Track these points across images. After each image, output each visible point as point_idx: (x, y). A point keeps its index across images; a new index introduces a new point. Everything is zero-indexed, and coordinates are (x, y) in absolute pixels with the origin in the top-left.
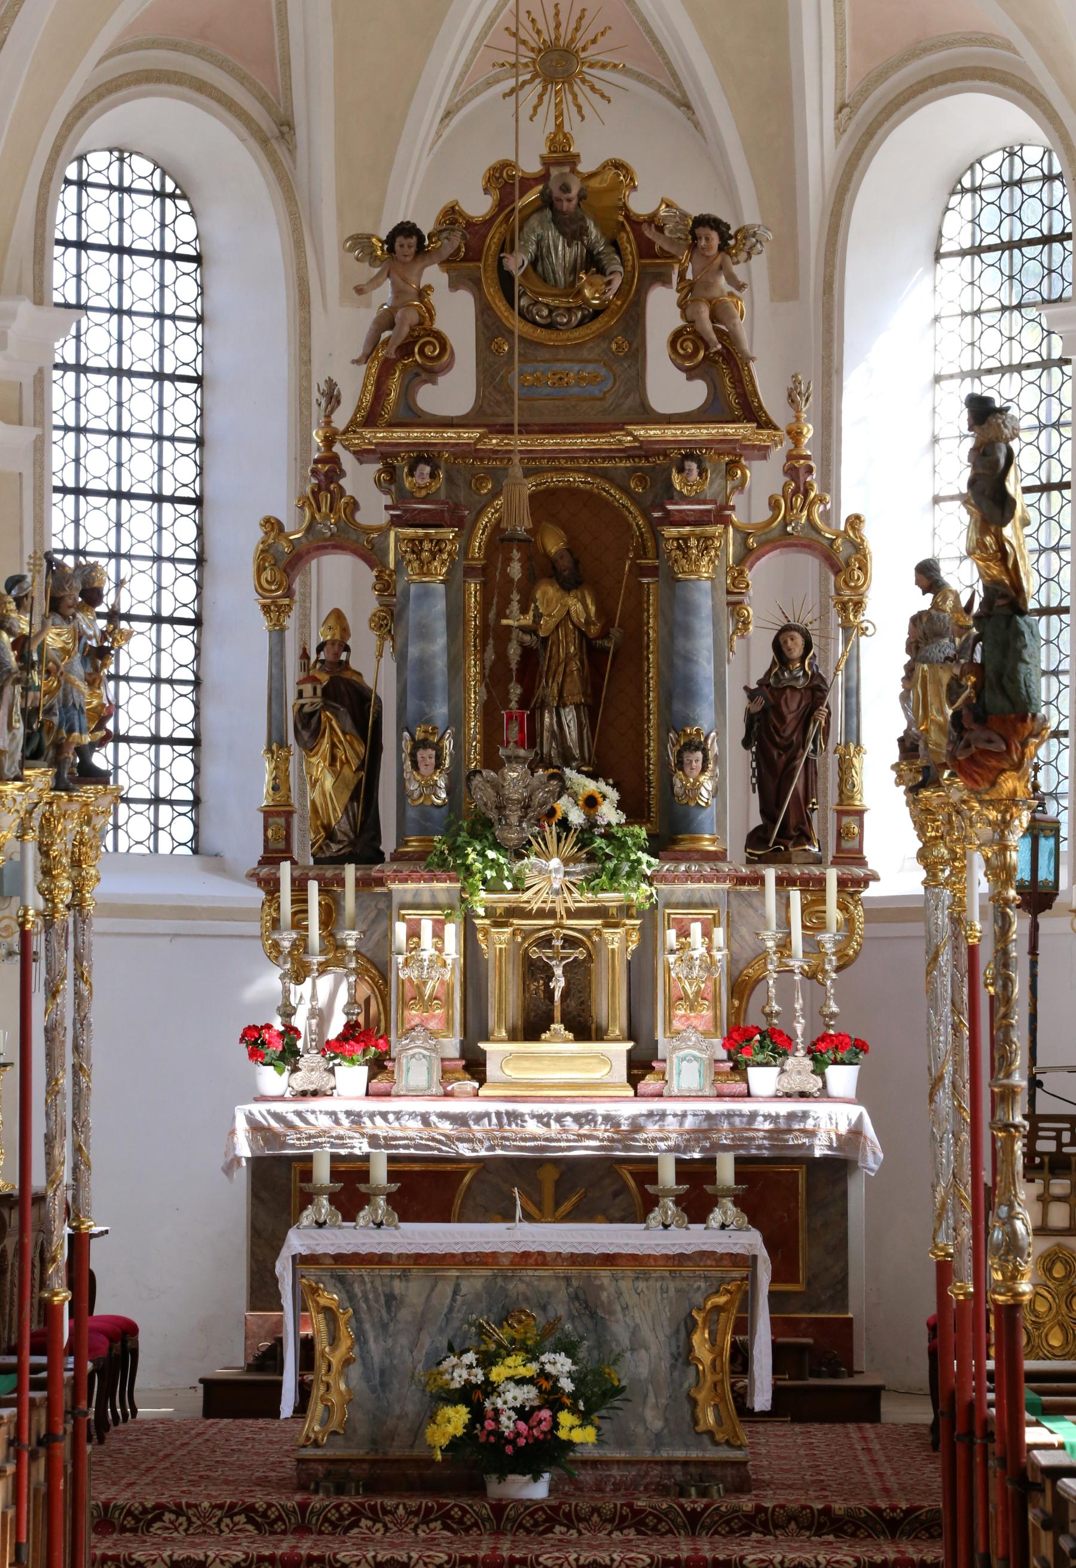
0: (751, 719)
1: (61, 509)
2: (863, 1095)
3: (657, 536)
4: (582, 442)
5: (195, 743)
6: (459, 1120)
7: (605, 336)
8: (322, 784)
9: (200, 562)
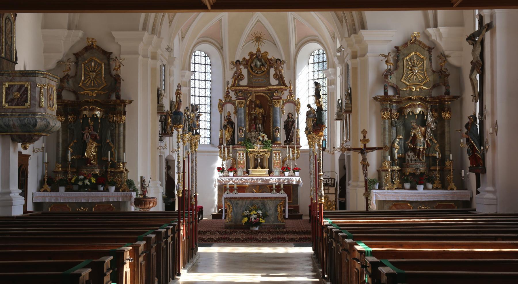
0: (285, 125)
1: (192, 98)
2: (300, 176)
3: (272, 101)
4: (261, 89)
5: (210, 129)
6: (246, 180)
7: (265, 75)
8: (227, 135)
9: (211, 105)
